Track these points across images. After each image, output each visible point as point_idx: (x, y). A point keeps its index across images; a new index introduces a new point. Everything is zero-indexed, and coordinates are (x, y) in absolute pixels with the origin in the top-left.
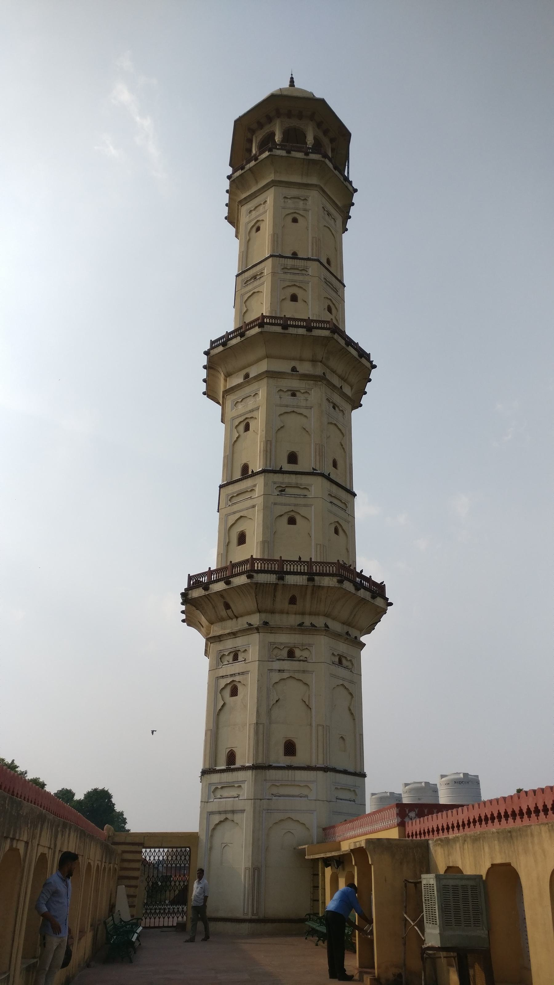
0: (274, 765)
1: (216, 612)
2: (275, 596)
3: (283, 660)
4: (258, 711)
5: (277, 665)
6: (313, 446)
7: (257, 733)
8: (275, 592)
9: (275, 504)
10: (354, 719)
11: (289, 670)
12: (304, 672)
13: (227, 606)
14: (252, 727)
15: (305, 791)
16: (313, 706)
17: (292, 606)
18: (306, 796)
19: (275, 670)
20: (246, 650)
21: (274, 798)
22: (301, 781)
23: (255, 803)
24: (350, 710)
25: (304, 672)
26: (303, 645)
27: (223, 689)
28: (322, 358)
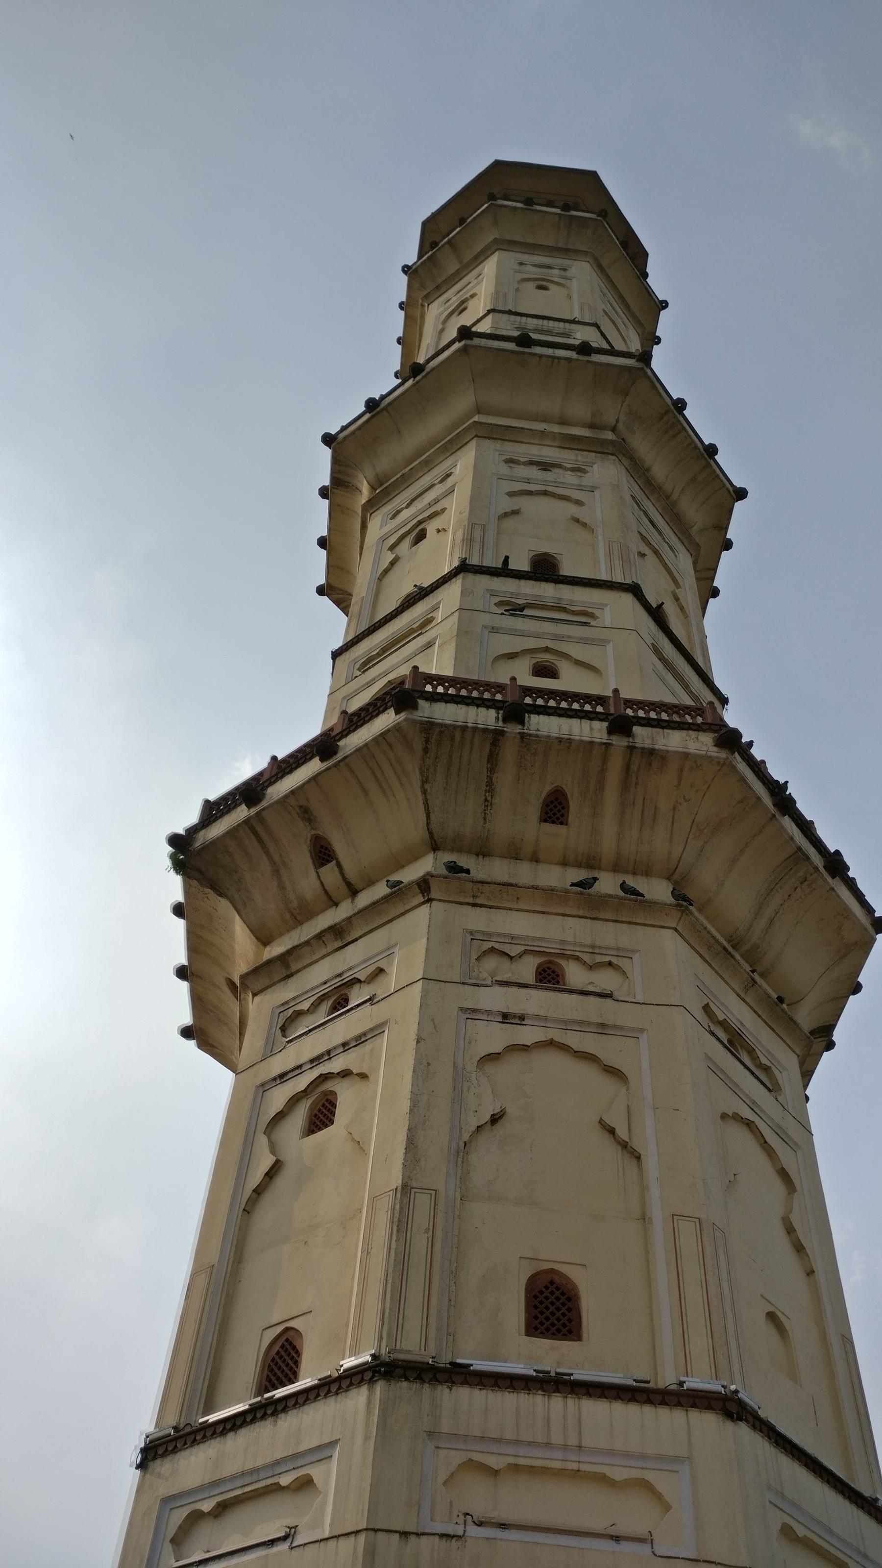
0: (479, 1365)
1: (282, 887)
2: (490, 787)
3: (525, 986)
4: (411, 1144)
5: (495, 999)
6: (601, 545)
7: (401, 1224)
8: (492, 770)
9: (494, 630)
10: (810, 1273)
11: (545, 1018)
12: (602, 1028)
13: (323, 853)
14: (385, 1205)
15: (633, 1514)
16: (647, 1141)
17: (548, 827)
18: (646, 1540)
19: (489, 1012)
20: (381, 971)
21: (473, 1531)
22: (611, 1452)
23: (371, 1553)
24: (790, 1230)
25: (602, 1028)
26: (593, 949)
27: (281, 1116)
28: (617, 421)
